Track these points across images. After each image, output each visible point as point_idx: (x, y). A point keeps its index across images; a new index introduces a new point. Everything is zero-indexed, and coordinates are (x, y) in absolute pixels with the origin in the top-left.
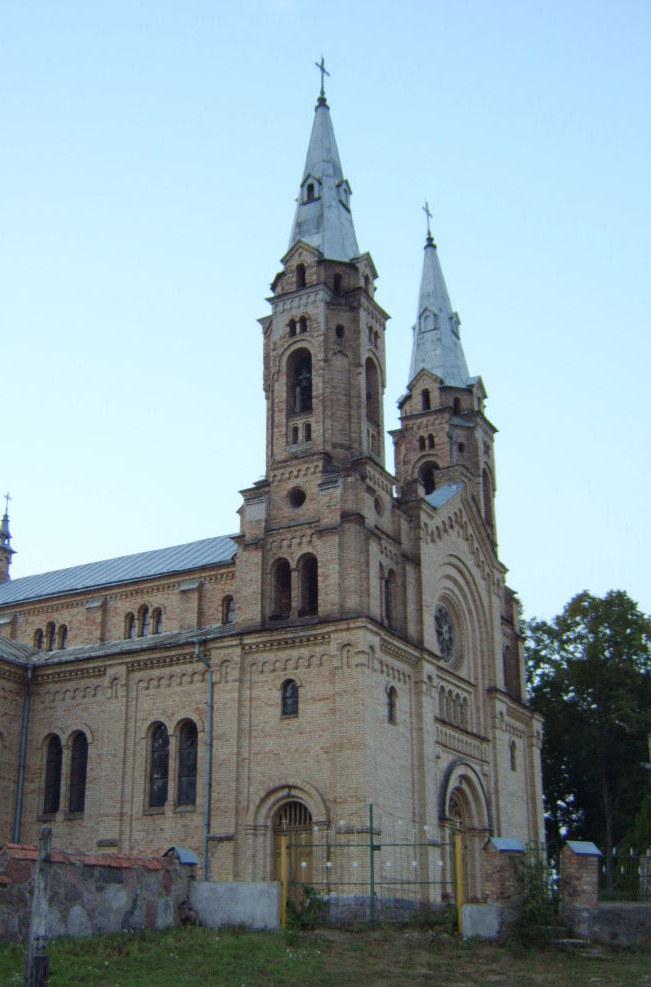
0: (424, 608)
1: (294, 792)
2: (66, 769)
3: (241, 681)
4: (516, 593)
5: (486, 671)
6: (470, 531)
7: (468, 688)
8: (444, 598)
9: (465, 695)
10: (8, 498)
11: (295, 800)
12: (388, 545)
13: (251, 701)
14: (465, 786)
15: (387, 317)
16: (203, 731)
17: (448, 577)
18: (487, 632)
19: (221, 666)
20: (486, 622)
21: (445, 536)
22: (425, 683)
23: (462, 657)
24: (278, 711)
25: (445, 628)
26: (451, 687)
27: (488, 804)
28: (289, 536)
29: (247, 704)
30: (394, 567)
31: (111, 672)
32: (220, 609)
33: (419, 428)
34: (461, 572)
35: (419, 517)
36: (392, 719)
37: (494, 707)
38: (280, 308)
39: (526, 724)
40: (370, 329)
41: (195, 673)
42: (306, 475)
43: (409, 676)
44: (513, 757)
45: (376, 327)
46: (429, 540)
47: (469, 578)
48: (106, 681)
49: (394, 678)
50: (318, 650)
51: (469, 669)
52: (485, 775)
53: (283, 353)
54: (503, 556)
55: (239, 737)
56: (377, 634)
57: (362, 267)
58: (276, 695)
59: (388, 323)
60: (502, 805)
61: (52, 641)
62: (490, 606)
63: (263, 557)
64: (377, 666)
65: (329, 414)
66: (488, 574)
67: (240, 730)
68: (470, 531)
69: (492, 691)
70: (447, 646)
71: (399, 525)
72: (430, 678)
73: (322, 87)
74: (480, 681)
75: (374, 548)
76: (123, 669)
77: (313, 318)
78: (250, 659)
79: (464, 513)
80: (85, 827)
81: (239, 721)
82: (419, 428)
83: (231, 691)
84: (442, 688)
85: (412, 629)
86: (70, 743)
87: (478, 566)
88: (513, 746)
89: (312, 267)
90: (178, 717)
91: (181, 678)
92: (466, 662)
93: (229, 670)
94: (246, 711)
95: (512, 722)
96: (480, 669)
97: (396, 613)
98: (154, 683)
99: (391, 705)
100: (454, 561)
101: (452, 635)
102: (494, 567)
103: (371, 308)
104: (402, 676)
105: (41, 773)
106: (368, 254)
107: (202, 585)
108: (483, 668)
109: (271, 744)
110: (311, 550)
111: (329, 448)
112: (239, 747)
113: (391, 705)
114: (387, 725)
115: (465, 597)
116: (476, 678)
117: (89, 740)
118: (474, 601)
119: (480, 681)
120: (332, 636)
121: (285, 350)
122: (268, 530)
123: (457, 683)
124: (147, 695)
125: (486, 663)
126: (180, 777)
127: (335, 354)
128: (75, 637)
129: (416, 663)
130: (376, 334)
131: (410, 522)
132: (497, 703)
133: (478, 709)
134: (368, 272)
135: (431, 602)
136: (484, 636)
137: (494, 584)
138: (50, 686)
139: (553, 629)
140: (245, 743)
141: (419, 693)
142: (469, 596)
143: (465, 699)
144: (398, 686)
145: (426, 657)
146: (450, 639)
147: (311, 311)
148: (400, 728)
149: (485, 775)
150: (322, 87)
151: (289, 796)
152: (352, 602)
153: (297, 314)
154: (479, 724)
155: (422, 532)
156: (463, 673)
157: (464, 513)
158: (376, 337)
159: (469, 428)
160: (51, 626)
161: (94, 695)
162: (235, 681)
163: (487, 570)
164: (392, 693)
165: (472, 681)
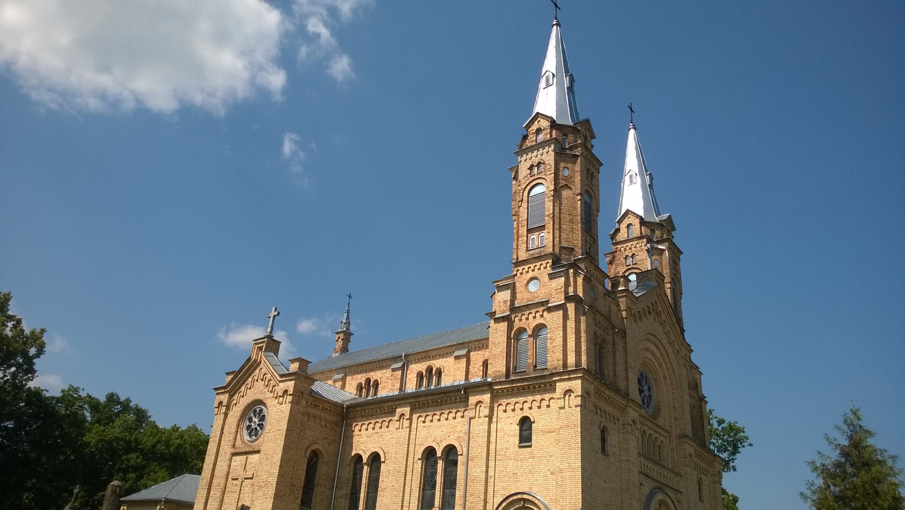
0: (629, 368)
6: (664, 318)
9: (662, 438)
10: (350, 297)
16: (462, 455)
17: (647, 349)
23: (659, 410)
24: (517, 440)
25: (646, 388)
32: (481, 368)
42: (539, 269)
43: (618, 420)
50: (547, 396)
52: (679, 502)
53: (526, 187)
61: (368, 391)
68: (664, 318)
71: (610, 308)
72: (634, 421)
83: (482, 424)
87: (670, 344)
89: (547, 129)
90: (444, 444)
97: (608, 371)
99: (603, 440)
100: (651, 337)
101: (650, 394)
103: (589, 156)
104: (612, 418)
105: (348, 483)
106: (588, 121)
107: (469, 352)
109: (511, 465)
110: (543, 322)
113: (603, 440)
114: (600, 455)
115: (660, 366)
116: (671, 427)
117: (382, 460)
120: (557, 384)
126: (444, 489)
129: (623, 410)
130: (592, 174)
146: (650, 396)
149: (679, 502)
153: (535, 161)
162: (485, 417)
165: (667, 428)
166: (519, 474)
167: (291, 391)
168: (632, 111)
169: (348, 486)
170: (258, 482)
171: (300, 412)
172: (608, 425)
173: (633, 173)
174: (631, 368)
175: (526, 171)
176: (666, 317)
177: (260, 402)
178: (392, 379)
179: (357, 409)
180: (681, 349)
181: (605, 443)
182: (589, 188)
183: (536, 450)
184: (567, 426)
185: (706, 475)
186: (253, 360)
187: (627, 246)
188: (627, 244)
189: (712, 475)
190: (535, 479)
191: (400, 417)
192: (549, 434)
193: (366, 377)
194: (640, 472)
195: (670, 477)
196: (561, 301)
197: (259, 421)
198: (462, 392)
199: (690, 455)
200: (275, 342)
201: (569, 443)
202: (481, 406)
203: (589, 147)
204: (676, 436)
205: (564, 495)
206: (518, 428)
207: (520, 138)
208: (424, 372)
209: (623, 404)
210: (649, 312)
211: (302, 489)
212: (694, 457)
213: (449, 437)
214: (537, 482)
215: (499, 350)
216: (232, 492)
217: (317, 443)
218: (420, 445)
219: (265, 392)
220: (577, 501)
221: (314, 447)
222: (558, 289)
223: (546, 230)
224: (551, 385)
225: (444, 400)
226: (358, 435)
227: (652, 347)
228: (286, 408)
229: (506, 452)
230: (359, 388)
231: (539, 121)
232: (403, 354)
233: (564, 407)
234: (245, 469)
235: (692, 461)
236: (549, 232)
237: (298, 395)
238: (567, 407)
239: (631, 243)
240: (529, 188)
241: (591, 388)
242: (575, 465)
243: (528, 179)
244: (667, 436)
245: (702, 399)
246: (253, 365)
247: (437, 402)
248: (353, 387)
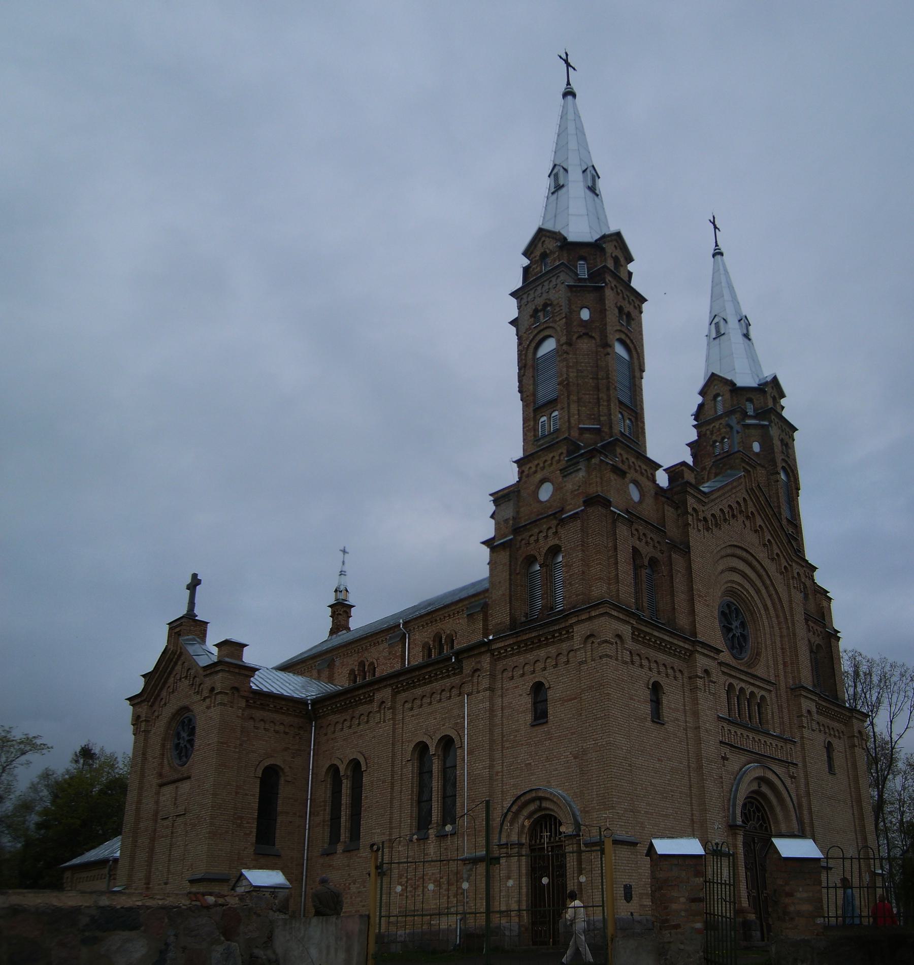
0: (696, 597)
1: (545, 804)
2: (345, 800)
3: (491, 689)
4: (829, 592)
5: (789, 669)
7: (768, 687)
8: (730, 592)
10: (344, 551)
11: (547, 812)
12: (647, 532)
13: (502, 709)
14: (765, 789)
15: (644, 300)
17: (733, 570)
18: (788, 628)
19: (472, 676)
20: (786, 619)
21: (725, 526)
22: (701, 678)
23: (758, 654)
24: (529, 717)
26: (752, 689)
28: (536, 530)
29: (499, 713)
33: (712, 434)
34: (760, 576)
35: (685, 503)
36: (657, 717)
38: (524, 301)
39: (845, 724)
40: (620, 309)
41: (453, 687)
45: (786, 438)
46: (701, 528)
47: (761, 571)
49: (830, 735)
50: (565, 646)
51: (768, 667)
54: (811, 556)
55: (491, 749)
56: (628, 623)
57: (609, 248)
58: (526, 701)
59: (645, 306)
60: (814, 809)
63: (510, 556)
64: (815, 726)
65: (575, 398)
66: (785, 567)
67: (492, 742)
68: (759, 522)
69: (797, 690)
73: (716, 242)
74: (782, 678)
75: (623, 531)
77: (555, 303)
78: (500, 666)
79: (749, 502)
80: (361, 857)
81: (491, 732)
82: (712, 434)
84: (731, 685)
85: (683, 621)
86: (349, 773)
87: (773, 559)
89: (554, 253)
91: (441, 694)
93: (480, 678)
94: (497, 720)
95: (821, 719)
96: (781, 667)
98: (418, 702)
99: (830, 759)
102: (793, 560)
108: (785, 664)
110: (557, 542)
111: (575, 434)
112: (492, 759)
114: (649, 724)
115: (758, 591)
116: (777, 676)
118: (770, 596)
119: (782, 678)
121: (530, 342)
122: (516, 531)
123: (752, 681)
124: (413, 716)
125: (788, 659)
127: (579, 337)
130: (629, 315)
131: (677, 508)
132: (803, 700)
133: (780, 708)
134: (618, 253)
136: (785, 632)
137: (793, 578)
138: (330, 718)
140: (498, 755)
141: (694, 689)
142: (764, 591)
143: (763, 697)
145: (699, 649)
147: (554, 296)
149: (792, 777)
150: (716, 242)
151: (540, 809)
152: (599, 590)
153: (540, 301)
154: (782, 723)
155: (690, 518)
156: (760, 671)
157: (749, 502)
159: (763, 426)
160: (362, 664)
161: (367, 722)
162: (485, 690)
163: (784, 563)
164: (656, 689)
166: (533, 764)
168: (717, 228)
169: (325, 810)
170: (191, 820)
171: (238, 717)
172: (663, 681)
173: (720, 318)
174: (700, 596)
175: (529, 320)
176: (763, 521)
177: (186, 709)
178: (391, 659)
180: (791, 566)
181: (660, 707)
182: (623, 337)
183: (553, 727)
185: (840, 738)
186: (170, 652)
187: (715, 426)
188: (713, 424)
189: (848, 737)
190: (554, 768)
191: (380, 707)
192: (569, 703)
193: (359, 660)
194: (721, 742)
195: (776, 745)
197: (188, 735)
198: (453, 660)
199: (809, 712)
200: (198, 622)
201: (594, 712)
202: (479, 676)
203: (625, 278)
204: (787, 688)
205: (589, 785)
208: (431, 643)
209: (688, 649)
210: (734, 516)
211: (255, 821)
212: (815, 716)
213: (444, 725)
214: (557, 772)
215: (501, 592)
216: (163, 837)
217: (272, 757)
218: (409, 742)
219: (190, 695)
220: (590, 791)
221: (267, 763)
222: (575, 490)
223: (559, 406)
224: (568, 632)
225: (432, 675)
226: (332, 739)
227: (742, 566)
229: (516, 736)
230: (352, 677)
231: (544, 241)
232: (401, 621)
233: (586, 661)
234: (175, 804)
235: (813, 720)
236: (563, 408)
238: (589, 660)
239: (719, 422)
240: (533, 345)
242: (602, 740)
243: (532, 332)
244: (771, 688)
246: (172, 659)
247: (424, 679)
248: (344, 676)
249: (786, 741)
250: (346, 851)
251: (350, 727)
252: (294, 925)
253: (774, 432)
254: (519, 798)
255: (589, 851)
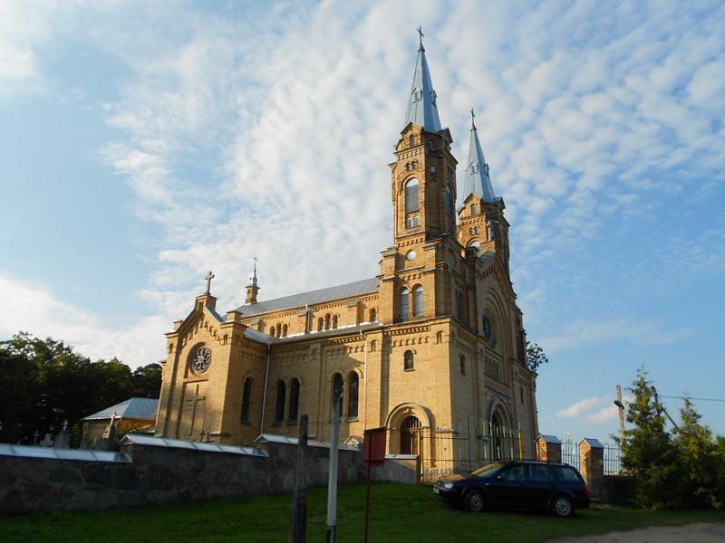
2: (287, 399)
8: (486, 310)
10: (256, 259)
17: (488, 299)
24: (403, 366)
25: (487, 326)
27: (511, 420)
30: (462, 292)
31: (312, 347)
34: (495, 298)
36: (463, 372)
37: (512, 368)
44: (522, 396)
48: (310, 351)
62: (509, 316)
70: (488, 335)
76: (319, 345)
85: (472, 324)
88: (522, 390)
92: (497, 345)
98: (336, 352)
99: (462, 365)
100: (491, 291)
106: (448, 129)
113: (462, 365)
114: (460, 376)
116: (503, 353)
126: (349, 402)
128: (292, 330)
135: (481, 311)
139: (462, 481)
141: (476, 359)
144: (466, 355)
147: (418, 158)
148: (467, 377)
153: (411, 160)
158: (452, 172)
160: (279, 326)
167: (230, 335)
179: (109, 457)
184: (439, 356)
196: (299, 332)
206: (403, 358)
207: (398, 141)
221: (247, 377)
228: (228, 348)
237: (236, 337)
241: (455, 329)
245: (522, 333)
249: (507, 386)
250: (288, 425)
251: (292, 361)
252: (638, 502)
253: (501, 227)
254: (398, 407)
255: (432, 438)
